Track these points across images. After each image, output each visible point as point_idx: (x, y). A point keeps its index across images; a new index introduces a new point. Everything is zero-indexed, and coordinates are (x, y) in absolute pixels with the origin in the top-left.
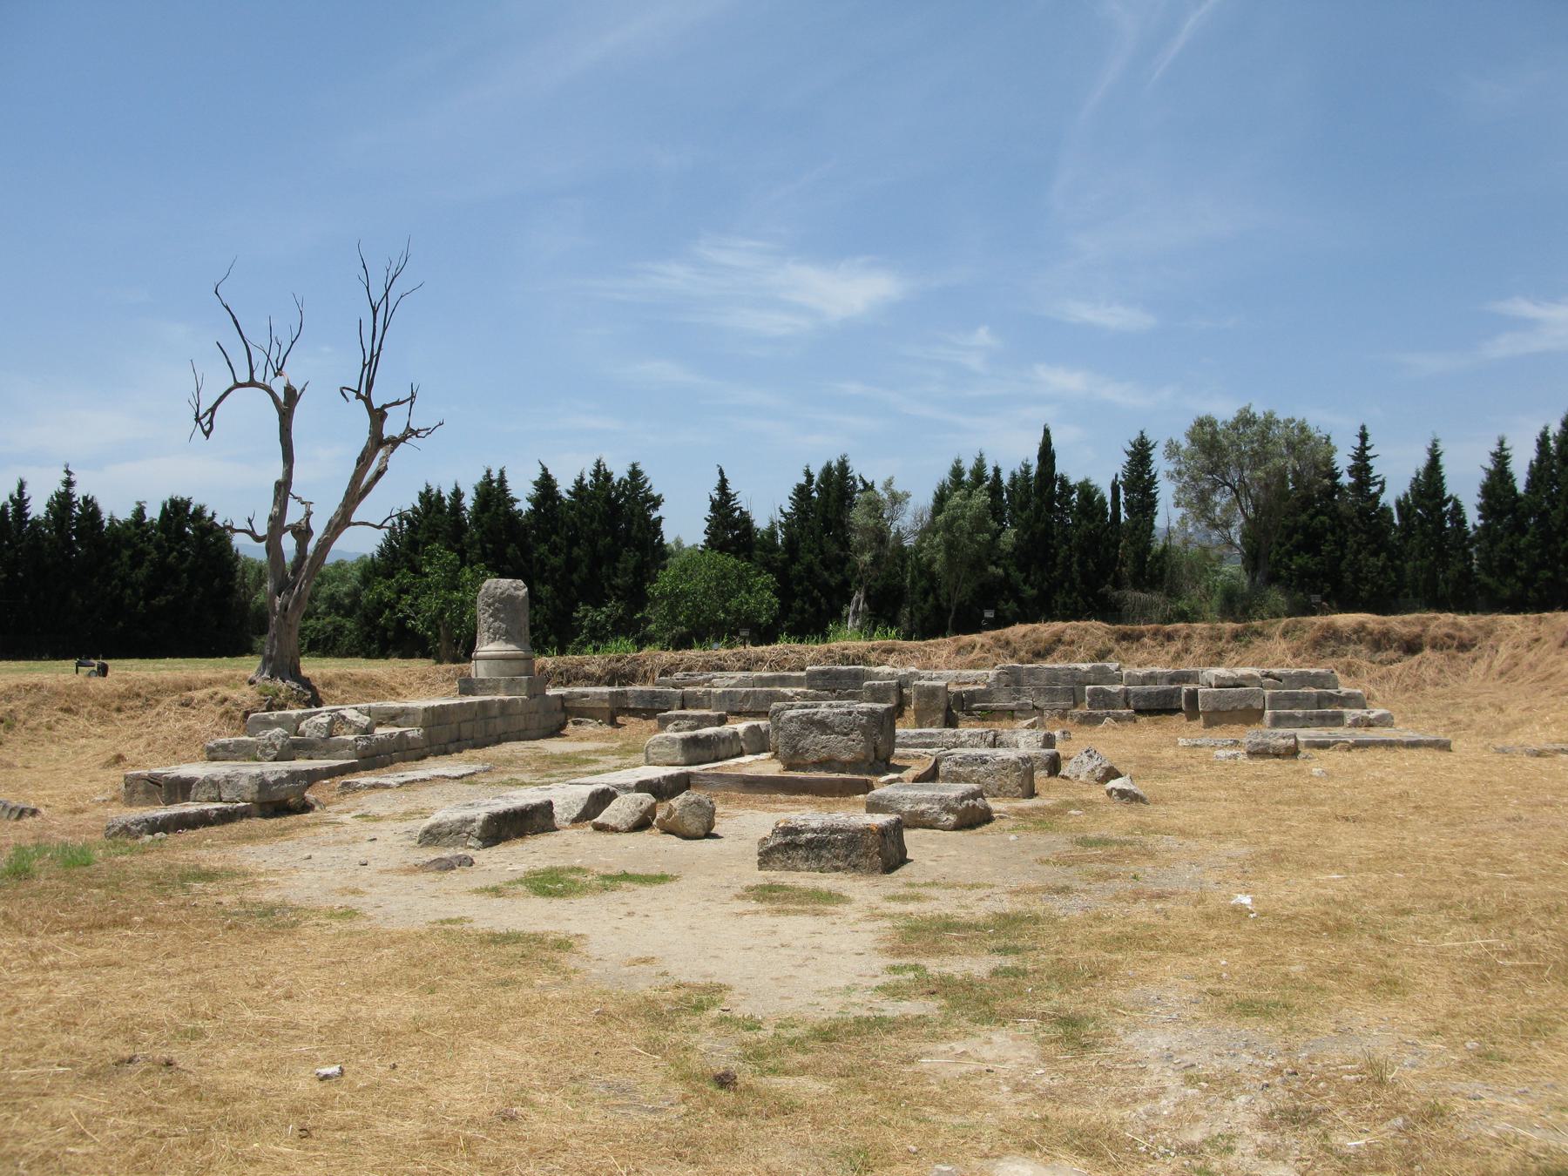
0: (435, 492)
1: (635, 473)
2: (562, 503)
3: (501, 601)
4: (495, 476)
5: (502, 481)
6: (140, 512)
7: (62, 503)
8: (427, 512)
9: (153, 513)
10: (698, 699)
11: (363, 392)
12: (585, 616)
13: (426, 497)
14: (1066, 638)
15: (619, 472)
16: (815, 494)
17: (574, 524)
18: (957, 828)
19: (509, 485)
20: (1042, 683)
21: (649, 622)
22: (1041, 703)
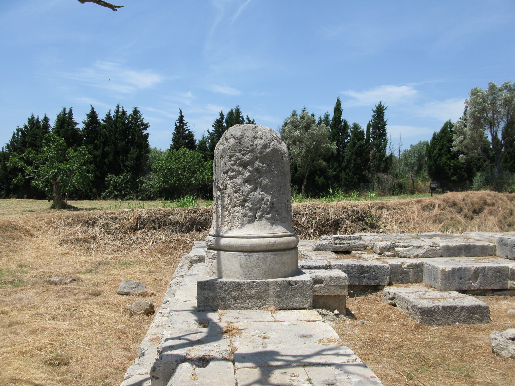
1: (136, 112)
2: (100, 125)
4: (67, 111)
5: (71, 114)
10: (403, 273)
12: (111, 180)
13: (31, 121)
14: (488, 201)
15: (129, 112)
17: (106, 135)
19: (74, 116)
21: (143, 183)
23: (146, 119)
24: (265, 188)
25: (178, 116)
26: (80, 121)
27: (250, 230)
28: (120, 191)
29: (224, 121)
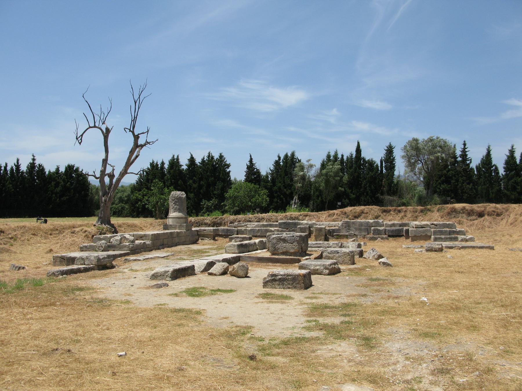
1: (221, 156)
2: (197, 167)
4: (176, 157)
5: (178, 159)
6: (58, 169)
7: (32, 166)
9: (62, 169)
11: (132, 130)
12: (205, 204)
13: (152, 164)
14: (365, 211)
15: (216, 156)
16: (282, 164)
19: (180, 160)
20: (357, 226)
22: (356, 233)
23: (228, 161)
24: (177, 205)
26: (184, 163)
27: (174, 214)
29: (281, 161)
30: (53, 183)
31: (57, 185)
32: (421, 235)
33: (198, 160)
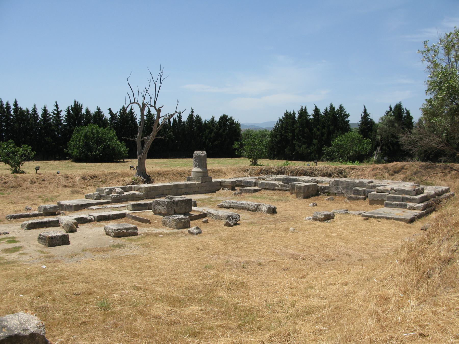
0: (289, 112)
1: (341, 107)
3: (197, 157)
4: (304, 108)
5: (305, 110)
6: (213, 119)
7: (191, 117)
8: (286, 118)
9: (217, 119)
11: (153, 104)
12: (326, 149)
13: (287, 114)
15: (337, 108)
18: (114, 237)
20: (345, 186)
25: (363, 110)
26: (310, 112)
28: (331, 156)
30: (207, 131)
31: (210, 133)
32: (378, 200)
33: (322, 111)
